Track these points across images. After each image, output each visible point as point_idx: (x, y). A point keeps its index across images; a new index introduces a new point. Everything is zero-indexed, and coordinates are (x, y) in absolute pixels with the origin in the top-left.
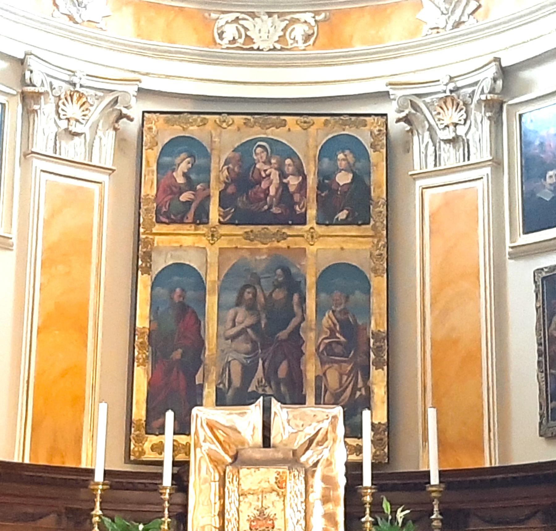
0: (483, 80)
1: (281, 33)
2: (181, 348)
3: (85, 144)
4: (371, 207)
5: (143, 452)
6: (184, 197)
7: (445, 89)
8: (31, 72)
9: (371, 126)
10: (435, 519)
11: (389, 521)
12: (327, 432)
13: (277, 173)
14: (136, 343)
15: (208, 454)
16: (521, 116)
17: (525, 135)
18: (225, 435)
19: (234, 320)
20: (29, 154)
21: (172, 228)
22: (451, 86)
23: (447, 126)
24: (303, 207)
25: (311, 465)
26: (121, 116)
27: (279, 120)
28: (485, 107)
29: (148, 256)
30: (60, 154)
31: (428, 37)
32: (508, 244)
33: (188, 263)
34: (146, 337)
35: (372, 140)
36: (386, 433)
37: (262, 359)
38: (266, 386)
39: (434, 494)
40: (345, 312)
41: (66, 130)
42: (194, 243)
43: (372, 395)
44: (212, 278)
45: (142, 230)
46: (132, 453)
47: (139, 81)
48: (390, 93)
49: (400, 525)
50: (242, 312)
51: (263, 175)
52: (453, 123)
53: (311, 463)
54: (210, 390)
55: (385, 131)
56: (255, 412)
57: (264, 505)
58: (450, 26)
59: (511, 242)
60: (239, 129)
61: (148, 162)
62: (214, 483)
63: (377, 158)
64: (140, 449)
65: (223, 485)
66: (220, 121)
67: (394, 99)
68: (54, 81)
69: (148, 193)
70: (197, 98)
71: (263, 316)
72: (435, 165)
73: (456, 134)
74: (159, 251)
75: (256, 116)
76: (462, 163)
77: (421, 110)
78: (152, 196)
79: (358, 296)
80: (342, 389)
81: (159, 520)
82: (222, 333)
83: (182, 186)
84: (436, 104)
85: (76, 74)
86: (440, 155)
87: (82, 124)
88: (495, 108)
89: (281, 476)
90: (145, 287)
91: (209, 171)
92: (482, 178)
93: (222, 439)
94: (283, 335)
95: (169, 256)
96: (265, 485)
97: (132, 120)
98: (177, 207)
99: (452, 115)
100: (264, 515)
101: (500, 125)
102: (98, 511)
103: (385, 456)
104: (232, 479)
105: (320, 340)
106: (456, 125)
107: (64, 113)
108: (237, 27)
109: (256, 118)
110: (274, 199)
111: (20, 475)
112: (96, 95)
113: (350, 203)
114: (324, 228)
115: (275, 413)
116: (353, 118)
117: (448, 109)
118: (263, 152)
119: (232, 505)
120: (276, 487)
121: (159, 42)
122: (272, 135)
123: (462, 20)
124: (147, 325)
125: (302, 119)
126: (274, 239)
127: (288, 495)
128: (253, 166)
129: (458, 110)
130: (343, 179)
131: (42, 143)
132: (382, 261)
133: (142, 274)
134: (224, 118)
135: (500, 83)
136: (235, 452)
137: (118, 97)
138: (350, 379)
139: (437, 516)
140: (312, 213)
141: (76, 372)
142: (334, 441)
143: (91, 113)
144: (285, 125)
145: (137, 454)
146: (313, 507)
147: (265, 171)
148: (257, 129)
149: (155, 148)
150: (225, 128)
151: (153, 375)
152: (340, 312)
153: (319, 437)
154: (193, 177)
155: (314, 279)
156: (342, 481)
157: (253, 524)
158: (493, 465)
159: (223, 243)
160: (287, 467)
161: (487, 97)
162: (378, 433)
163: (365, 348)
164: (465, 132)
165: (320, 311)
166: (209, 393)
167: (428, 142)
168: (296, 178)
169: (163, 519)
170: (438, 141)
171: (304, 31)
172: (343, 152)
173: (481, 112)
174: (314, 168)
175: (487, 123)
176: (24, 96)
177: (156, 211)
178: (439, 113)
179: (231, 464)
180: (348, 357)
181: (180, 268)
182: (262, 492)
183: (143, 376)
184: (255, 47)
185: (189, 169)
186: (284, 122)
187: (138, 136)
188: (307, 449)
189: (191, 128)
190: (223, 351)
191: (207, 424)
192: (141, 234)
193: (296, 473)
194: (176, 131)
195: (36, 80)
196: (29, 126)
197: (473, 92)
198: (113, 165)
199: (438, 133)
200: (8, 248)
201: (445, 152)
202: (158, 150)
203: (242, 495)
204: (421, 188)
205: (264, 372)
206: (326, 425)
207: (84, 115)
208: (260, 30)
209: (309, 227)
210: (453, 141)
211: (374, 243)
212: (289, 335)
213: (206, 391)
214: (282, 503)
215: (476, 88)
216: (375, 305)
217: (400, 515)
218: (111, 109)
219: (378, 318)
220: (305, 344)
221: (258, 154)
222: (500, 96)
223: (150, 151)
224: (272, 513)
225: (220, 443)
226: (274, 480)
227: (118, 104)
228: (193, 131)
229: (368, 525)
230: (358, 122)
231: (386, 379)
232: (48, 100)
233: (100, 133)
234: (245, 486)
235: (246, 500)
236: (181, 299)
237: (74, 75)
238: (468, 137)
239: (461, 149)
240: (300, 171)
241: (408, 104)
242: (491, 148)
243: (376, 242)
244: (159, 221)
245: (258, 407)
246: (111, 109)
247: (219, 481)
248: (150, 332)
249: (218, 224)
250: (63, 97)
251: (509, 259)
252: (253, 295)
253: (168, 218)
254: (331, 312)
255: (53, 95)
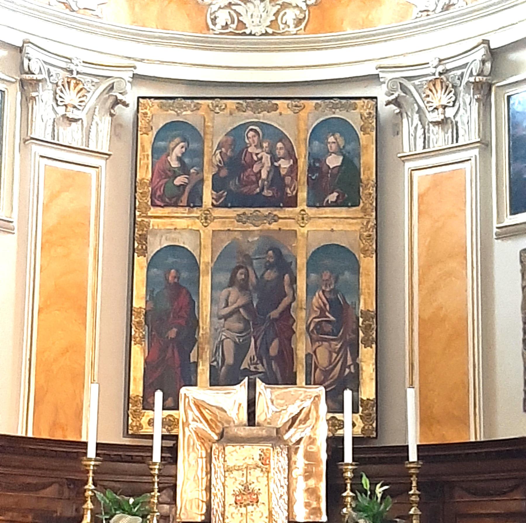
0: (473, 61)
1: (274, 18)
2: (175, 328)
3: (82, 130)
4: (361, 189)
5: (141, 427)
6: (178, 181)
7: (434, 72)
8: (29, 60)
9: (361, 109)
10: (413, 495)
11: (368, 496)
12: (310, 411)
13: (269, 156)
14: (133, 322)
15: (195, 432)
16: (509, 97)
17: (514, 117)
18: (211, 414)
19: (227, 301)
20: (28, 140)
21: (167, 211)
22: (440, 69)
23: (436, 108)
24: (294, 190)
25: (294, 442)
26: (117, 102)
27: (270, 105)
28: (473, 89)
29: (144, 238)
30: (58, 140)
31: (418, 20)
32: (495, 225)
33: (182, 245)
34: (143, 317)
35: (362, 123)
36: (375, 409)
37: (254, 338)
38: (258, 364)
39: (412, 471)
40: (334, 291)
41: (64, 116)
42: (188, 226)
43: (360, 372)
44: (206, 259)
45: (137, 213)
46: (130, 428)
47: (135, 68)
48: (380, 76)
49: (379, 500)
50: (234, 292)
51: (255, 158)
52: (442, 105)
53: (294, 440)
54: (204, 368)
55: (375, 114)
56: (240, 391)
57: (248, 481)
58: (439, 9)
59: (498, 223)
60: (231, 114)
61: (143, 147)
62: (201, 459)
63: (367, 140)
64: (138, 424)
65: (209, 461)
66: (213, 106)
67: (384, 83)
68: (52, 69)
69: (144, 177)
70: (191, 82)
71: (255, 295)
72: (424, 148)
73: (445, 117)
74: (155, 233)
75: (248, 101)
76: (450, 145)
77: (411, 92)
78: (148, 180)
79: (347, 275)
80: (331, 367)
81: (148, 494)
82: (216, 312)
83: (176, 169)
84: (425, 87)
85: (73, 61)
86: (429, 137)
87: (79, 110)
88: (484, 89)
89: (264, 453)
90: (142, 268)
91: (203, 154)
92: (470, 160)
93: (209, 417)
94: (275, 314)
95: (164, 238)
96: (250, 462)
97: (127, 105)
98: (172, 191)
99: (440, 98)
100: (249, 490)
101: (489, 106)
102: (90, 486)
103: (373, 431)
104: (218, 456)
105: (310, 319)
106: (444, 107)
107: (62, 100)
108: (229, 12)
109: (248, 102)
110: (266, 183)
111: (23, 448)
112: (92, 82)
113: (341, 185)
114: (314, 210)
115: (260, 393)
116: (344, 101)
117: (437, 91)
118: (255, 136)
119: (218, 480)
120: (260, 464)
121: (152, 28)
122: (264, 119)
123: (451, 3)
124: (143, 305)
125: (294, 103)
126: (265, 221)
127: (272, 471)
128: (246, 150)
129: (447, 92)
130: (334, 161)
131: (41, 130)
132: (371, 241)
133: (138, 256)
134: (217, 103)
135: (488, 65)
136: (221, 429)
137: (113, 84)
138: (339, 356)
139: (415, 491)
140: (303, 195)
141: (76, 349)
142: (317, 419)
143: (88, 98)
144: (277, 109)
145: (135, 428)
146: (297, 482)
147: (257, 154)
148: (249, 113)
149: (150, 133)
150: (218, 113)
151: (150, 353)
152: (330, 291)
153: (302, 416)
154: (187, 160)
155: (305, 261)
156: (324, 457)
157: (238, 498)
158: (478, 440)
159: (215, 225)
160: (271, 445)
161: (475, 79)
162: (367, 409)
163: (354, 327)
164: (454, 114)
165: (310, 291)
166: (203, 372)
167: (417, 125)
168: (288, 161)
169: (153, 494)
170: (427, 123)
171: (296, 15)
172: (333, 135)
173: (469, 94)
174: (304, 152)
175: (475, 106)
176: (22, 83)
177: (151, 195)
178: (428, 96)
179: (218, 441)
180: (336, 336)
181: (174, 249)
182: (247, 468)
183: (139, 352)
184: (248, 32)
185: (183, 154)
186: (275, 106)
187: (134, 122)
188: (290, 427)
189: (184, 113)
190: (216, 330)
191: (195, 404)
192: (137, 217)
193: (279, 450)
194: (170, 116)
195: (35, 68)
196: (28, 113)
197: (462, 74)
198: (109, 150)
199: (427, 116)
200: (9, 231)
201: (434, 134)
202: (153, 135)
203: (227, 471)
204: (410, 170)
205: (256, 351)
206: (307, 403)
207: (81, 102)
208: (252, 15)
209: (300, 209)
210: (442, 123)
211: (363, 224)
212: (281, 314)
213: (200, 368)
214: (266, 478)
215: (465, 70)
216: (364, 285)
217: (379, 490)
218: (107, 95)
219: (367, 297)
220: (295, 324)
221: (250, 138)
222: (488, 78)
223: (145, 135)
224: (256, 489)
225: (207, 421)
226: (259, 457)
227: (114, 91)
228: (187, 115)
229: (349, 499)
230: (348, 105)
231: (374, 357)
232: (46, 87)
233: (97, 118)
234: (230, 463)
235: (232, 476)
236: (176, 280)
237: (71, 63)
238: (457, 119)
239: (450, 130)
240: (291, 154)
241: (397, 86)
242: (479, 129)
243: (365, 224)
244: (154, 205)
245: (243, 387)
246: (107, 95)
247: (206, 457)
248: (146, 313)
249: (211, 207)
250: (60, 84)
251: (496, 239)
252: (245, 275)
253: (162, 201)
254: (321, 293)
255: (51, 82)
